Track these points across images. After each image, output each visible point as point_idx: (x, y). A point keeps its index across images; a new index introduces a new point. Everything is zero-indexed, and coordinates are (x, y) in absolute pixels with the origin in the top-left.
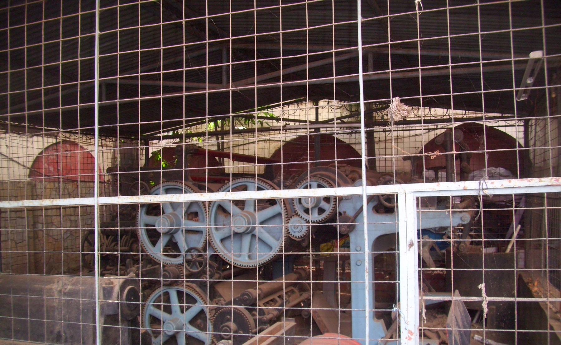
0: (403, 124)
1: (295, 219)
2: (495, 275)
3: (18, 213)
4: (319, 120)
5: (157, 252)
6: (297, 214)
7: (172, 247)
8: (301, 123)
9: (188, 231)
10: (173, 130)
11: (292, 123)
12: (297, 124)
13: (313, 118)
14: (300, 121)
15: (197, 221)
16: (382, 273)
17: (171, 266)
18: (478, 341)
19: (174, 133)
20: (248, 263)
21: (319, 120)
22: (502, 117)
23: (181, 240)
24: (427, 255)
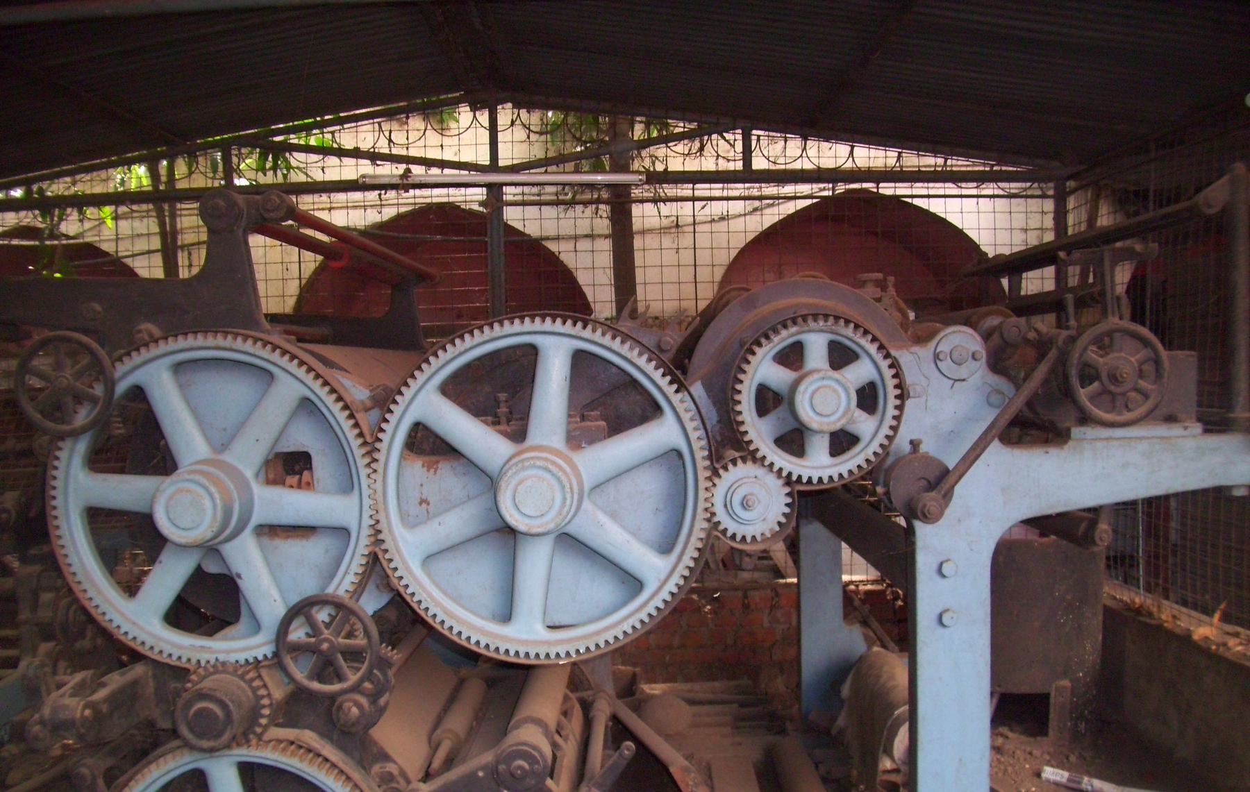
0: (744, 181)
1: (739, 474)
2: (1069, 597)
3: (137, 241)
4: (501, 163)
5: (141, 617)
6: (753, 456)
7: (210, 601)
8: (447, 171)
9: (271, 531)
10: (26, 184)
11: (417, 170)
12: (435, 171)
13: (485, 159)
14: (442, 164)
15: (309, 486)
16: (695, 597)
17: (216, 671)
18: (1057, 784)
19: (29, 192)
20: (548, 643)
21: (501, 163)
22: (980, 178)
23: (251, 563)
24: (293, 480)
